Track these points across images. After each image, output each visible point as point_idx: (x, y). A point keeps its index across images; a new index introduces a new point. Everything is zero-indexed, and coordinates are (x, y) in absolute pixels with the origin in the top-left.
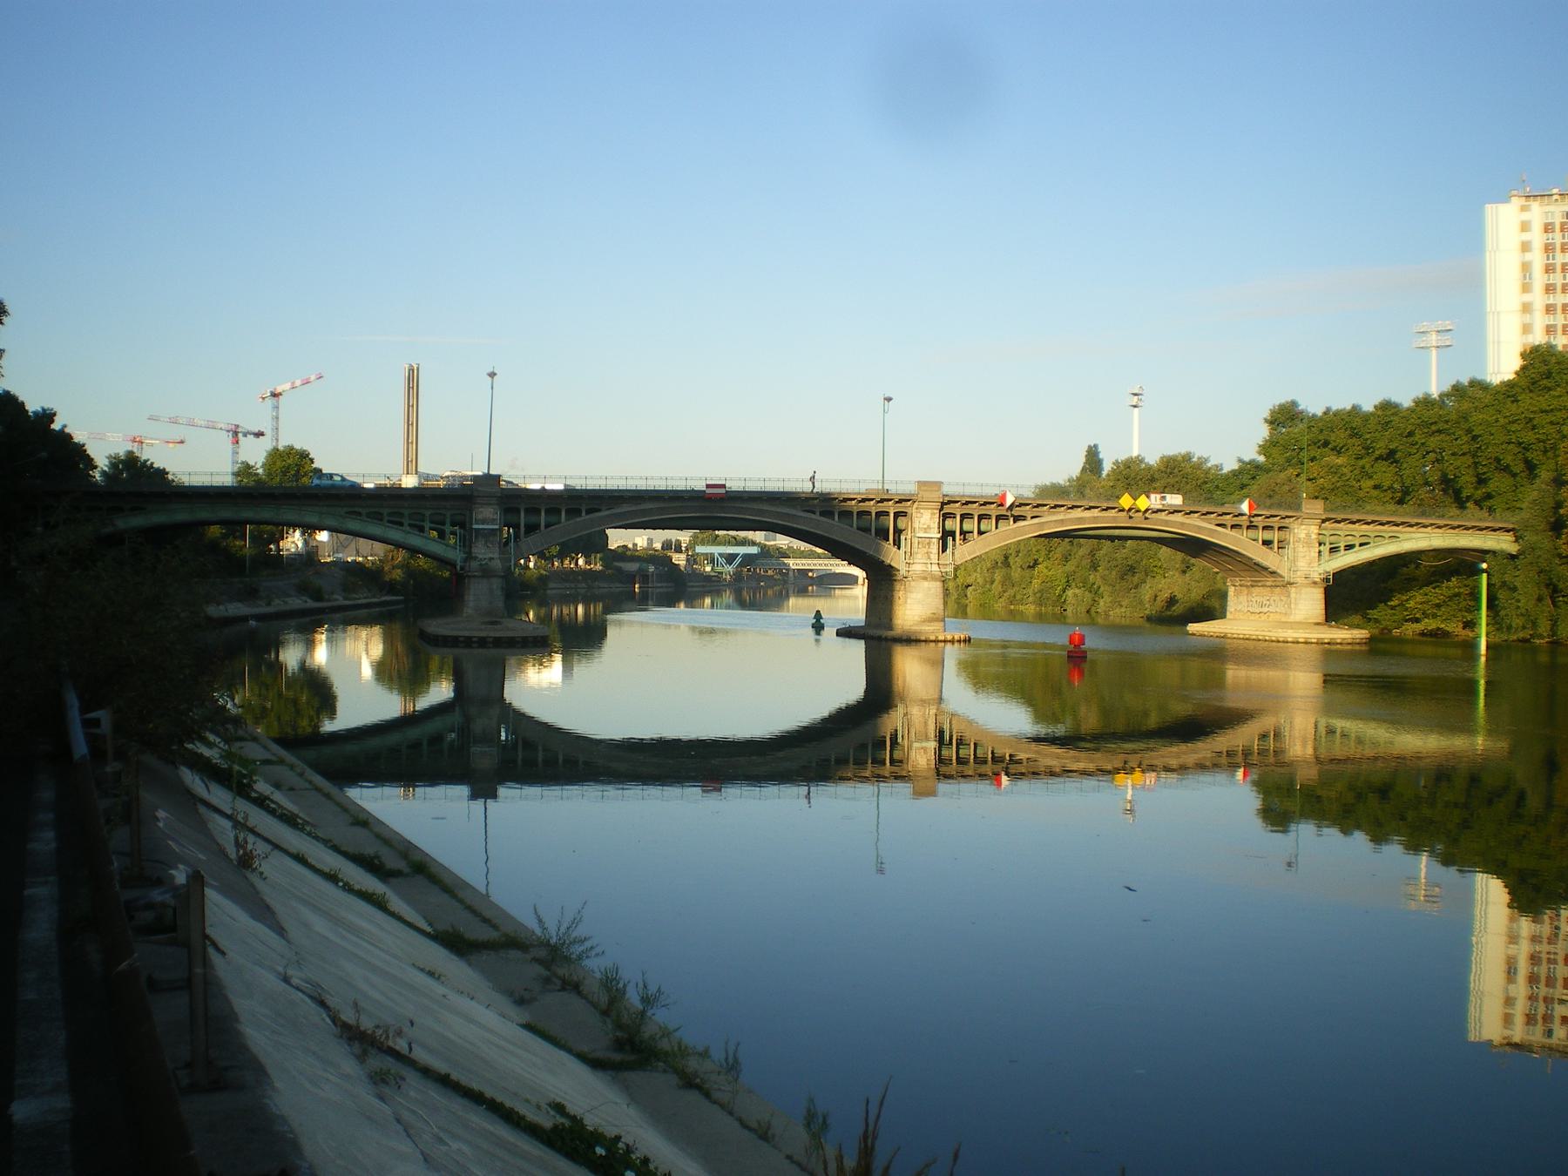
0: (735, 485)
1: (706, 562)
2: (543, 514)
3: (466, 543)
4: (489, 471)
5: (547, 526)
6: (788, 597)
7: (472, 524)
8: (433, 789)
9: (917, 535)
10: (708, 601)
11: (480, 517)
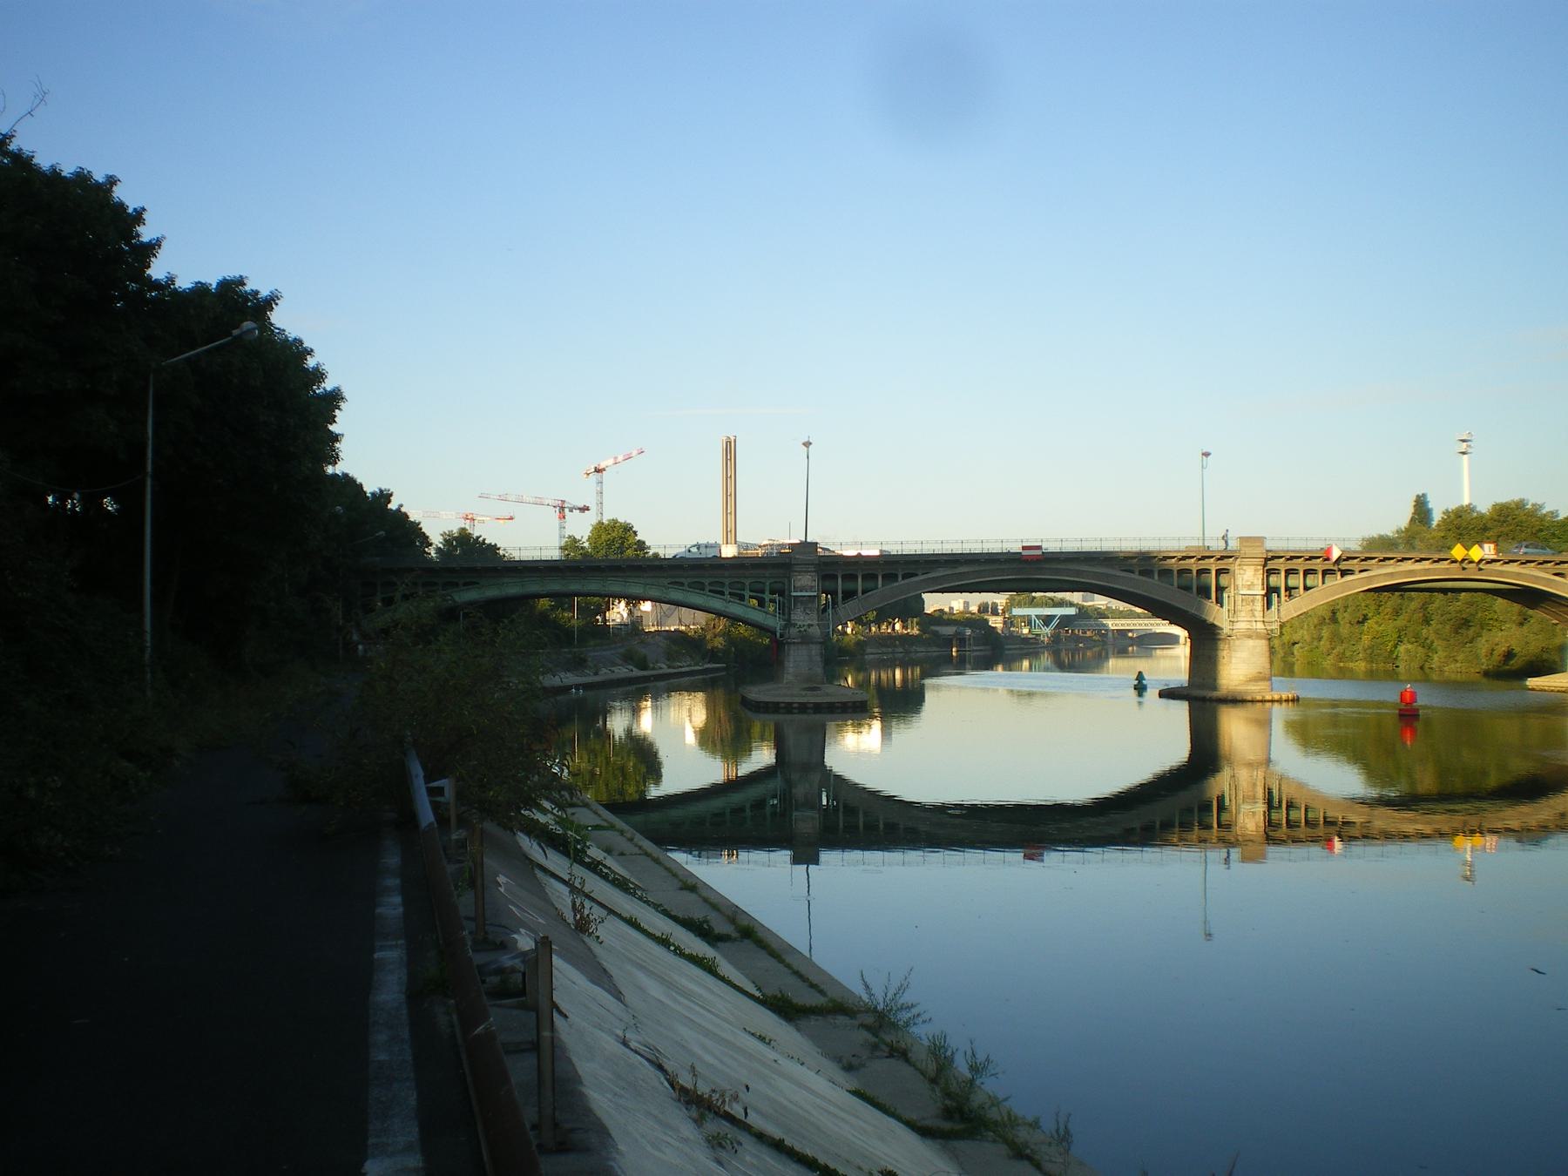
0: (1051, 546)
1: (1023, 624)
2: (860, 580)
5: (864, 592)
6: (1107, 658)
11: (798, 584)
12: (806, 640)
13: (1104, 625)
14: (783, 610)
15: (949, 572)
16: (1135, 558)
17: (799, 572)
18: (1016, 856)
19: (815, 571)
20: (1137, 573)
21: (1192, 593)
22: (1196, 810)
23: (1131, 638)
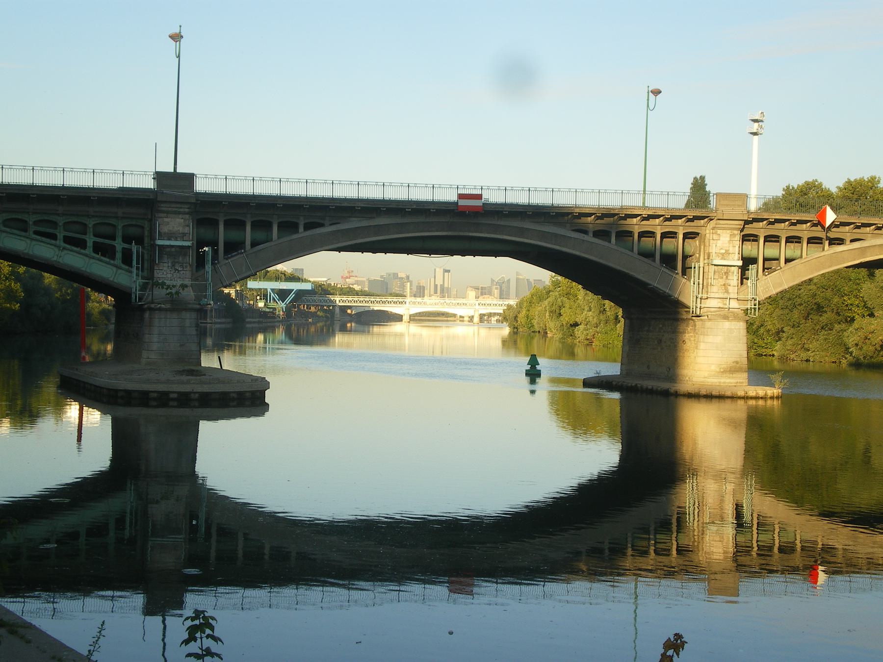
0: (494, 197)
1: (258, 298)
2: (248, 228)
3: (148, 268)
4: (175, 168)
5: (254, 244)
6: (334, 335)
10: (260, 337)
11: (165, 229)
12: (176, 305)
15: (365, 223)
16: (590, 215)
17: (167, 212)
18: (440, 591)
21: (654, 261)
22: (776, 550)
23: (350, 315)
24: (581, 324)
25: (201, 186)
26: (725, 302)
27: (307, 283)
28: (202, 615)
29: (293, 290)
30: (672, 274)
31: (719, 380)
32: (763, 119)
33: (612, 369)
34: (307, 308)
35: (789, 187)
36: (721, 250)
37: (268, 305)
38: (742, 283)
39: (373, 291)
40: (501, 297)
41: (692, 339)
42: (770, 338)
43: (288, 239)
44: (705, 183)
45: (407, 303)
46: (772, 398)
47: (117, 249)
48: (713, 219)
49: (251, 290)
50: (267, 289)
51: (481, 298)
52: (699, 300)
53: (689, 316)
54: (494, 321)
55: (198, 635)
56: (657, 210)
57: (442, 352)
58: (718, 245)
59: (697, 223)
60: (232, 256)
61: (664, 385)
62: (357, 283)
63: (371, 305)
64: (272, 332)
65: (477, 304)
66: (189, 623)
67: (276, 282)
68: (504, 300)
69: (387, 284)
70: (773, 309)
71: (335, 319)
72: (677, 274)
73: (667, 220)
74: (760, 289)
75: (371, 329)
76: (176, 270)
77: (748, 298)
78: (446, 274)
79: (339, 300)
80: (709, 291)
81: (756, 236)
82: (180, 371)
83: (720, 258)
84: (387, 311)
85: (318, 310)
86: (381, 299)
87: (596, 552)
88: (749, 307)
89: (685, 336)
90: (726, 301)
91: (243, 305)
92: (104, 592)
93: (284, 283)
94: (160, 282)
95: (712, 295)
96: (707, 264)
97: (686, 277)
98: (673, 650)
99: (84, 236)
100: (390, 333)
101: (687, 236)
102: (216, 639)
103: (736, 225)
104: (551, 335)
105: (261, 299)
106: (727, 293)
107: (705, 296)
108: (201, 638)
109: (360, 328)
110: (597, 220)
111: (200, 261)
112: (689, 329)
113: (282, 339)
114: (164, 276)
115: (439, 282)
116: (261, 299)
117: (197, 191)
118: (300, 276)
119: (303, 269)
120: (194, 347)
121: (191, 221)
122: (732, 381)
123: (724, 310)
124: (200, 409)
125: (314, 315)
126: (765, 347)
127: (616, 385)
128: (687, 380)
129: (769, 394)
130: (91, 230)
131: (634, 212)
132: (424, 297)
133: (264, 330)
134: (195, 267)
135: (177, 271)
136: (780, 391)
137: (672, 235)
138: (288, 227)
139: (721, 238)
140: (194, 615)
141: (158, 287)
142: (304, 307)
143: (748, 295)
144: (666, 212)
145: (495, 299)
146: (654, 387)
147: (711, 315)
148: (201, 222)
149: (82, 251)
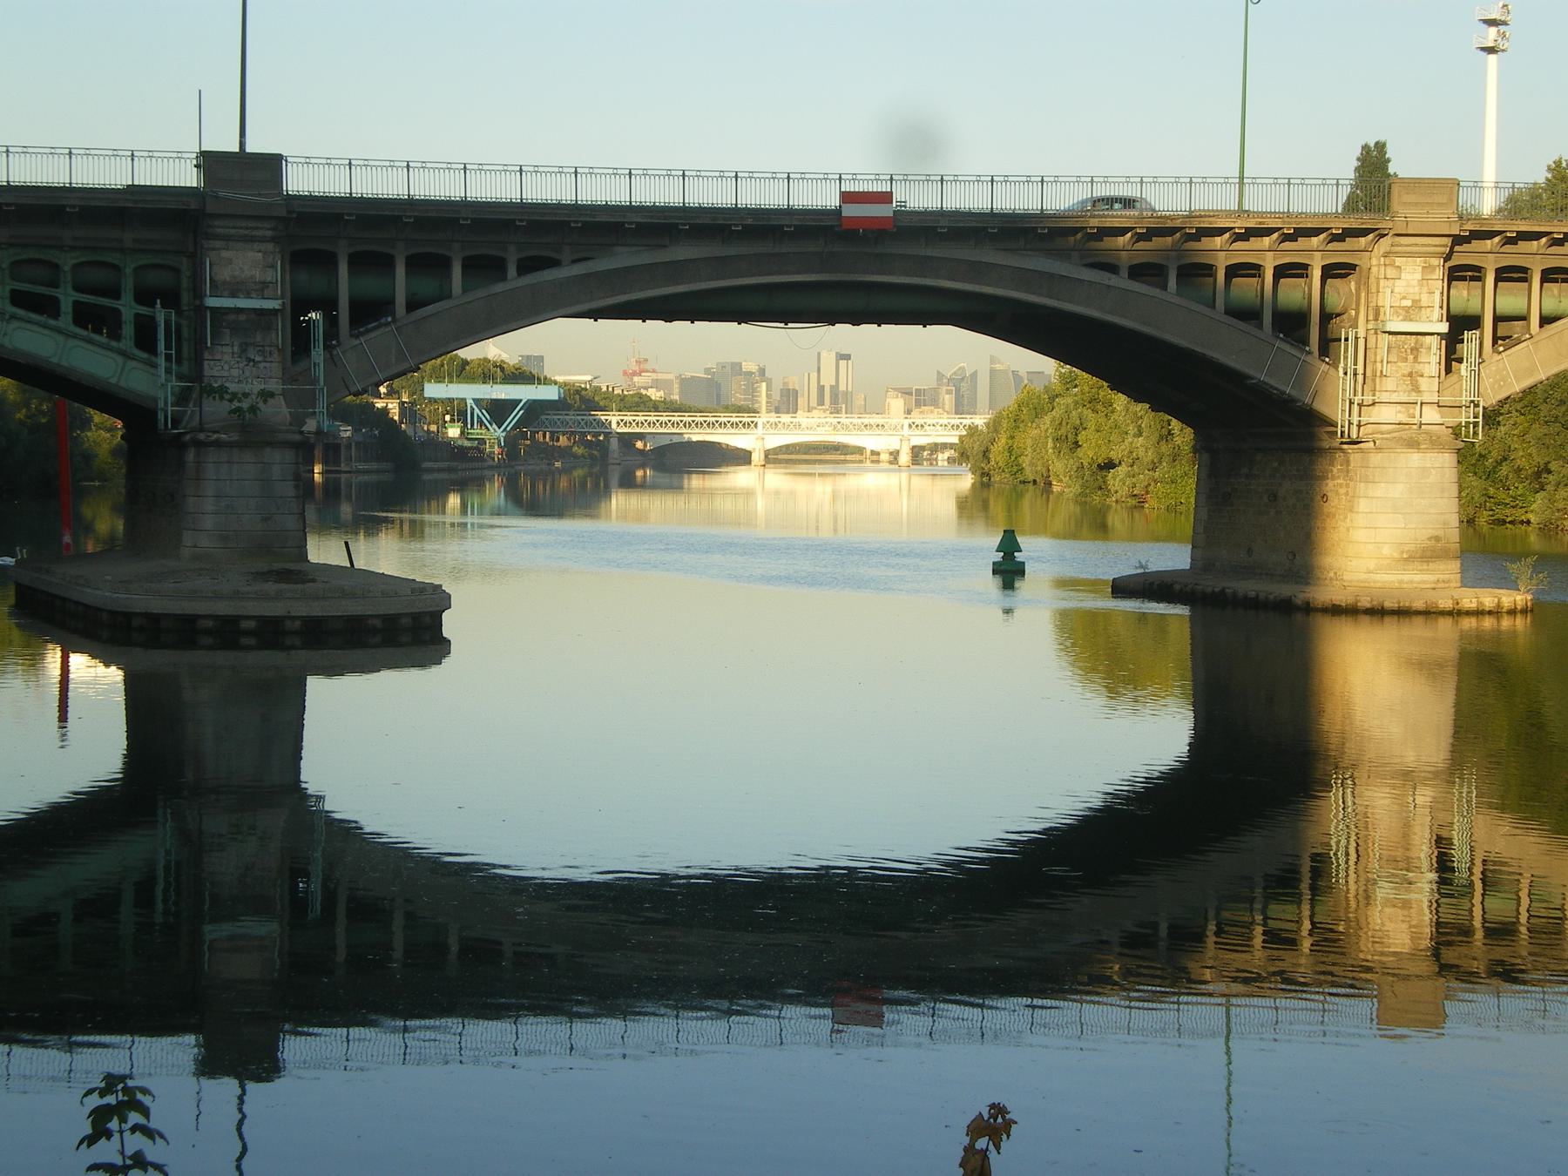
1: (448, 418)
2: (400, 271)
4: (242, 144)
5: (412, 306)
6: (607, 493)
7: (202, 297)
8: (212, 1082)
9: (1391, 327)
10: (454, 501)
11: (224, 274)
13: (601, 424)
14: (179, 351)
15: (646, 258)
17: (228, 238)
19: (273, 240)
20: (1124, 273)
21: (1260, 326)
23: (641, 452)
24: (1120, 463)
25: (298, 181)
26: (1411, 411)
27: (549, 386)
28: (121, 1085)
29: (521, 401)
30: (1299, 355)
31: (1400, 577)
32: (1508, 18)
33: (1174, 557)
34: (552, 439)
35: (1560, 162)
36: (1402, 301)
37: (468, 433)
38: (1448, 370)
39: (689, 402)
40: (959, 410)
41: (1342, 491)
42: (1521, 486)
43: (481, 293)
44: (1387, 156)
45: (760, 425)
46: (1512, 612)
47: (124, 318)
48: (1387, 234)
49: (433, 401)
50: (465, 399)
51: (915, 413)
52: (1355, 408)
53: (1336, 443)
54: (943, 460)
55: (114, 1124)
56: (1266, 217)
57: (835, 530)
58: (1396, 290)
59: (1350, 243)
60: (368, 331)
61: (1282, 590)
62: (656, 384)
63: (684, 431)
64: (479, 491)
65: (906, 427)
66: (95, 1101)
67: (485, 386)
68: (964, 416)
69: (718, 386)
70: (1526, 425)
71: (611, 461)
72: (1309, 353)
73: (1287, 238)
74: (1487, 382)
75: (686, 482)
76: (249, 360)
77: (1461, 401)
78: (843, 363)
79: (616, 421)
80: (1377, 389)
81: (1478, 269)
82: (263, 574)
83: (1401, 317)
84: (719, 443)
85: (574, 443)
86: (717, 419)
87: (1138, 942)
88: (1463, 420)
89: (1327, 485)
90: (1415, 408)
91: (416, 433)
92: (119, 1037)
93: (501, 386)
94: (216, 385)
95: (1384, 397)
96: (1373, 331)
97: (1327, 359)
98: (987, 1137)
99: (53, 290)
100: (724, 489)
101: (1330, 272)
102: (149, 1133)
103: (1436, 246)
104: (1059, 489)
105: (452, 421)
106: (1416, 392)
107: (1368, 399)
108: (121, 1132)
109: (664, 479)
110: (1137, 241)
111: (301, 341)
112: (1335, 470)
113: (499, 505)
114: (226, 374)
115: (828, 380)
116: (452, 421)
117: (290, 193)
118: (535, 372)
119: (543, 357)
120: (291, 523)
121: (278, 256)
122: (1426, 577)
123: (1410, 429)
124: (303, 652)
125: (565, 453)
126: (1512, 504)
127: (1181, 590)
128: (1331, 579)
129: (1506, 605)
130: (69, 278)
131: (1216, 223)
132: (796, 412)
133: (461, 486)
134: (289, 354)
135: (251, 364)
136: (1529, 597)
137: (1295, 270)
138: (485, 268)
139: (1403, 275)
140: (103, 1085)
141: (211, 398)
142: (544, 437)
143: (1461, 396)
144: (1284, 223)
145: (945, 415)
146: (1260, 594)
147: (1382, 439)
148: (299, 259)
149: (52, 322)
